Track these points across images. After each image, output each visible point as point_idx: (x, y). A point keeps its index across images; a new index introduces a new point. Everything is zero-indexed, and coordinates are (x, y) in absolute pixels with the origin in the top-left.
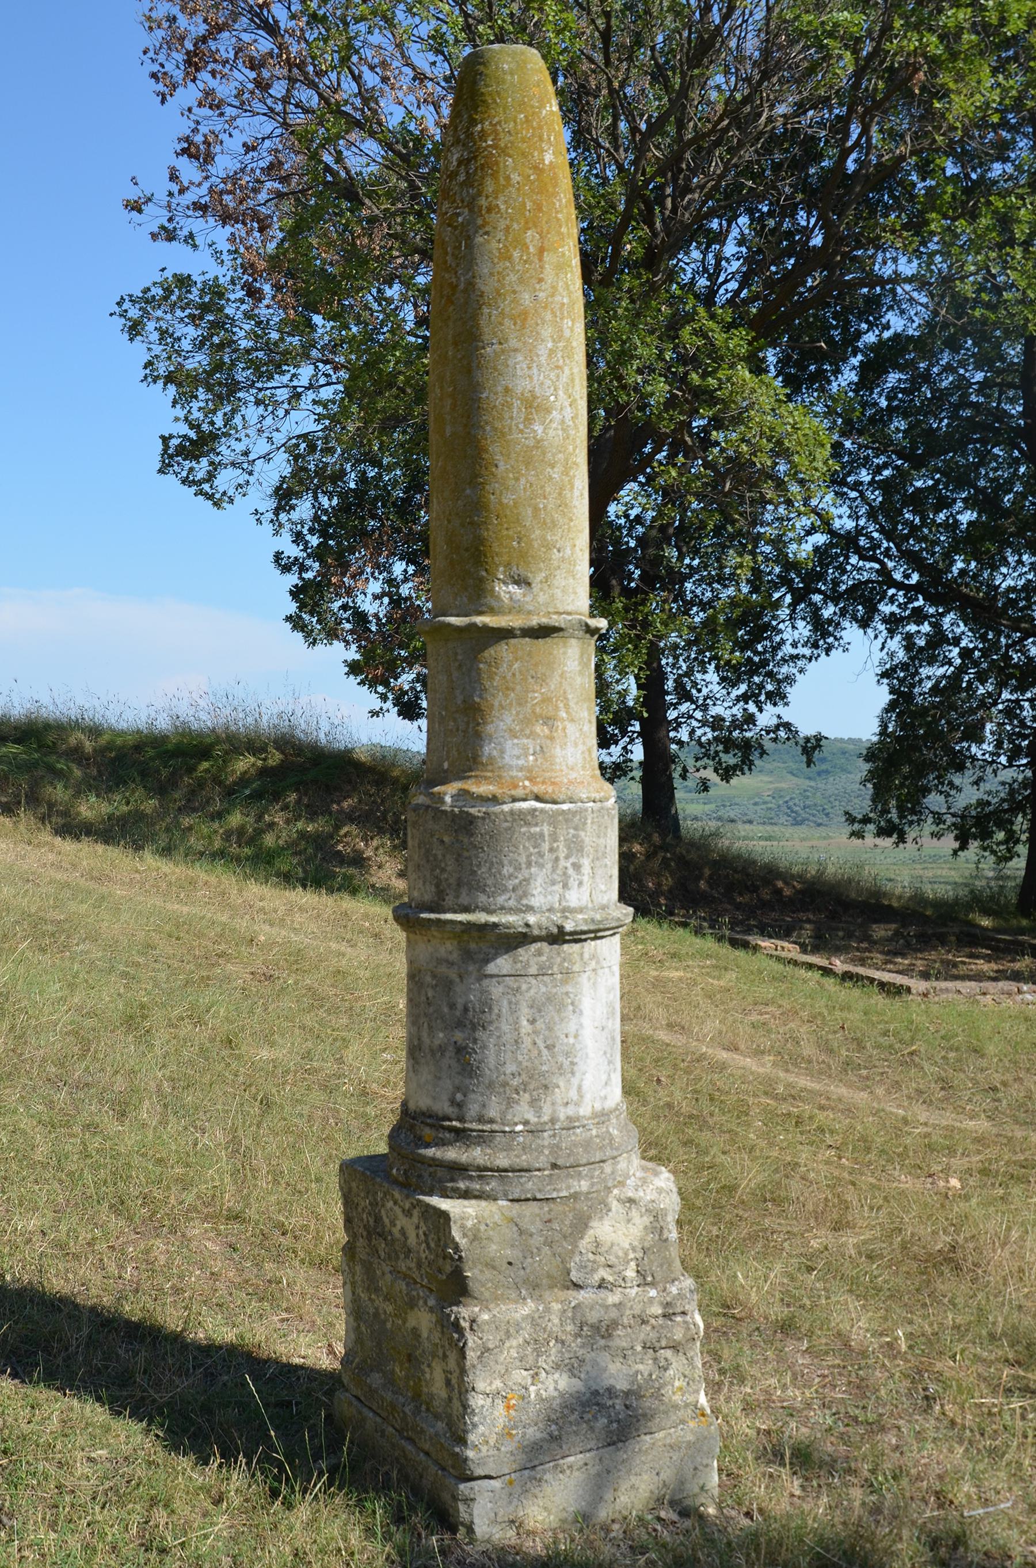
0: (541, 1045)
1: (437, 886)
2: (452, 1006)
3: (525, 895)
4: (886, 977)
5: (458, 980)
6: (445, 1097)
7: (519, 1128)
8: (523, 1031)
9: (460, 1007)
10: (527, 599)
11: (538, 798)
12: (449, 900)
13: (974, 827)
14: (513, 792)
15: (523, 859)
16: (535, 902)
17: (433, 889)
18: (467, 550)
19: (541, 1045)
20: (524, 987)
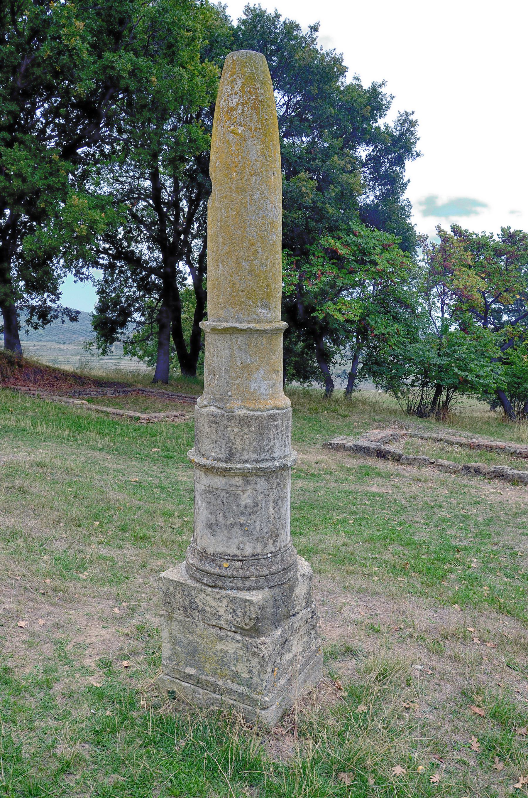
0: (277, 517)
1: (230, 451)
2: (238, 506)
3: (272, 452)
4: (132, 413)
5: (242, 494)
6: (234, 546)
7: (269, 555)
8: (271, 513)
9: (243, 506)
10: (269, 316)
11: (277, 409)
12: (237, 456)
13: (130, 348)
14: (268, 407)
15: (272, 437)
16: (276, 455)
17: (227, 452)
18: (243, 291)
19: (277, 517)
20: (271, 493)
